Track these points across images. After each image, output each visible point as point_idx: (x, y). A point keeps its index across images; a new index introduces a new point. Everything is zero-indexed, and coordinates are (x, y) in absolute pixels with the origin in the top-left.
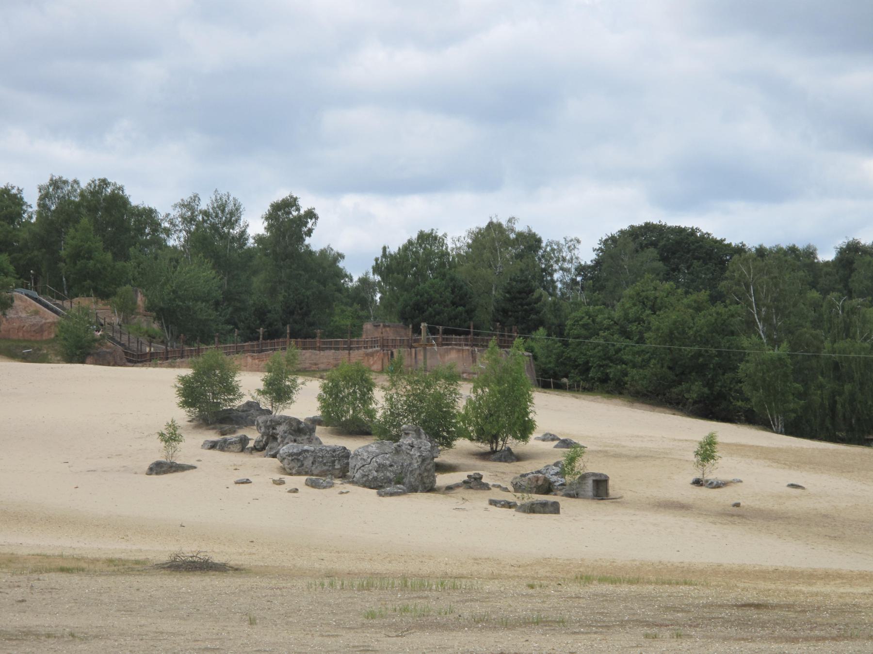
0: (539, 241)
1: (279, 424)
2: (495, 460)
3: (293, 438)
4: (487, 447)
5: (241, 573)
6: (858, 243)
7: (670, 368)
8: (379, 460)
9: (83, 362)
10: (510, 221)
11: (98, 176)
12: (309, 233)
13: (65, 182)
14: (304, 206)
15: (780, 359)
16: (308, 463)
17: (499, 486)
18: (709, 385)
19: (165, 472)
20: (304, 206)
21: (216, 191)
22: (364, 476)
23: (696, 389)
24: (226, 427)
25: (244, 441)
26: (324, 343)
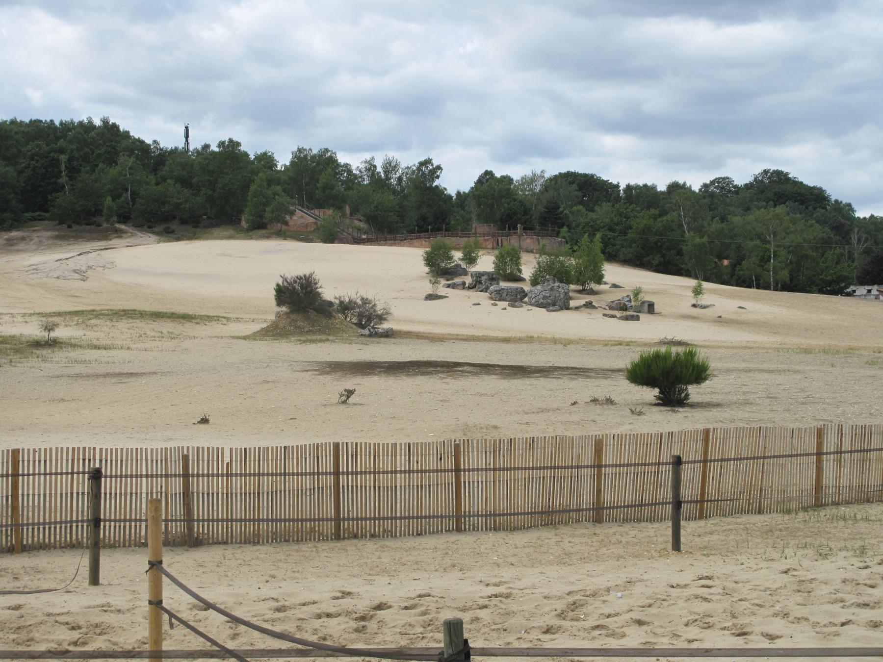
0: (512, 180)
1: (483, 275)
2: (586, 294)
3: (490, 282)
4: (580, 288)
5: (61, 348)
6: (678, 182)
7: (642, 248)
8: (544, 293)
9: (333, 242)
10: (542, 172)
11: (324, 147)
12: (438, 177)
13: (305, 150)
14: (435, 163)
15: (704, 244)
16: (504, 295)
17: (601, 307)
18: (663, 256)
19: (434, 299)
20: (435, 163)
21: (386, 155)
22: (536, 302)
23: (657, 259)
24: (450, 277)
25: (464, 283)
26: (463, 234)
